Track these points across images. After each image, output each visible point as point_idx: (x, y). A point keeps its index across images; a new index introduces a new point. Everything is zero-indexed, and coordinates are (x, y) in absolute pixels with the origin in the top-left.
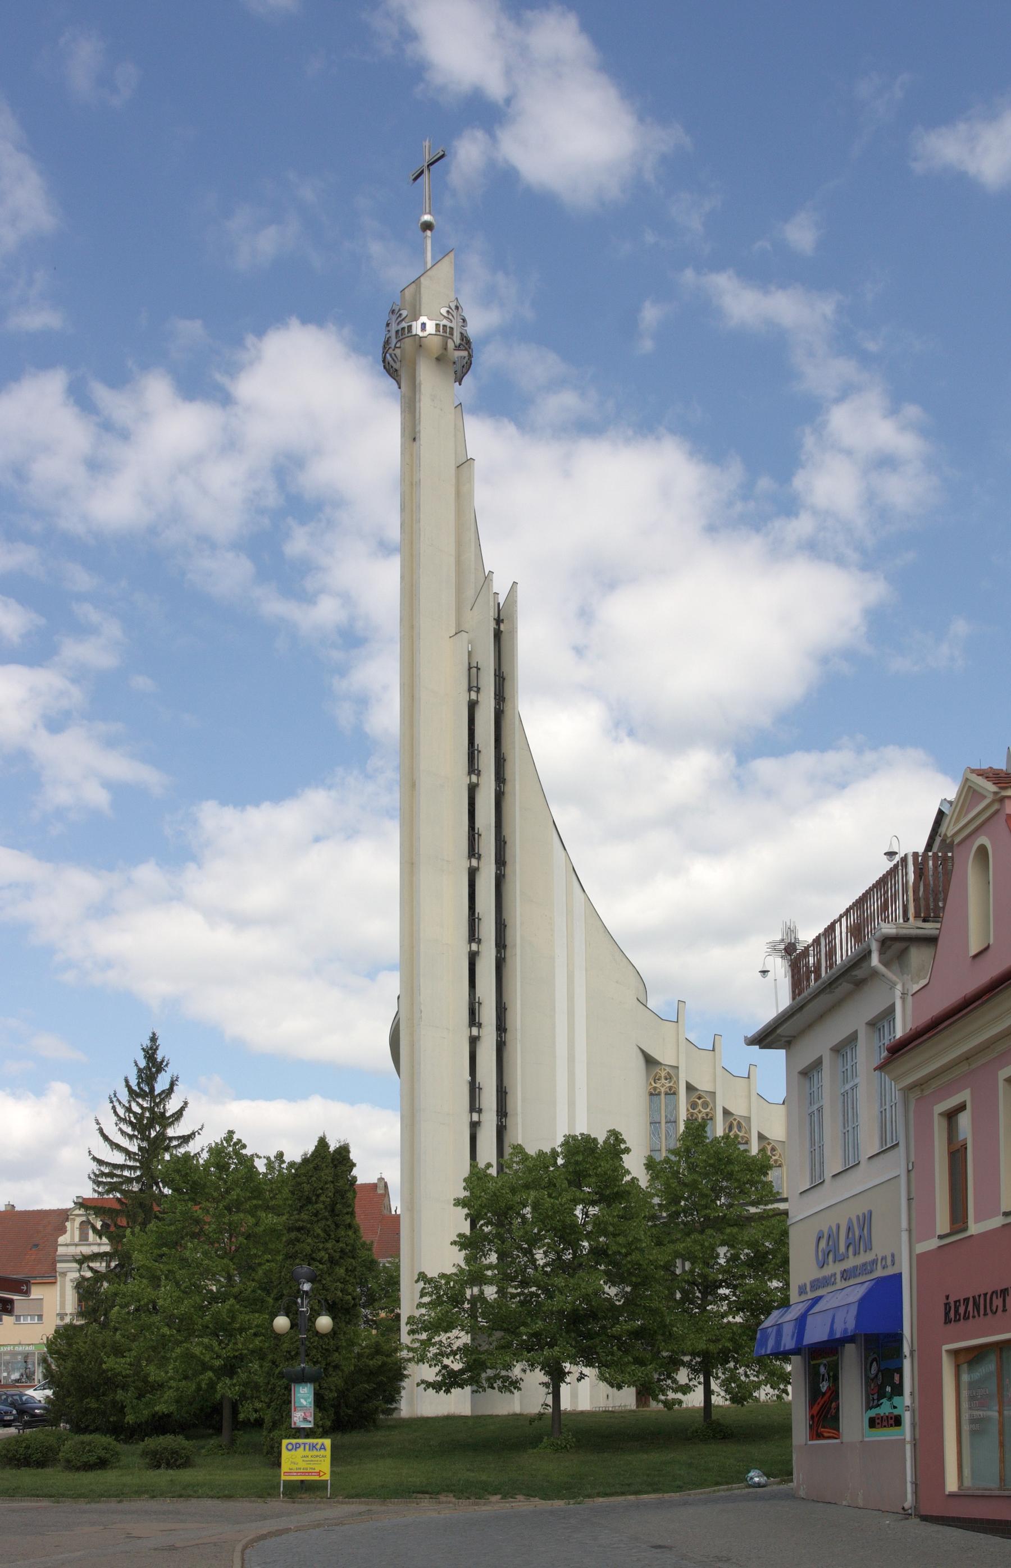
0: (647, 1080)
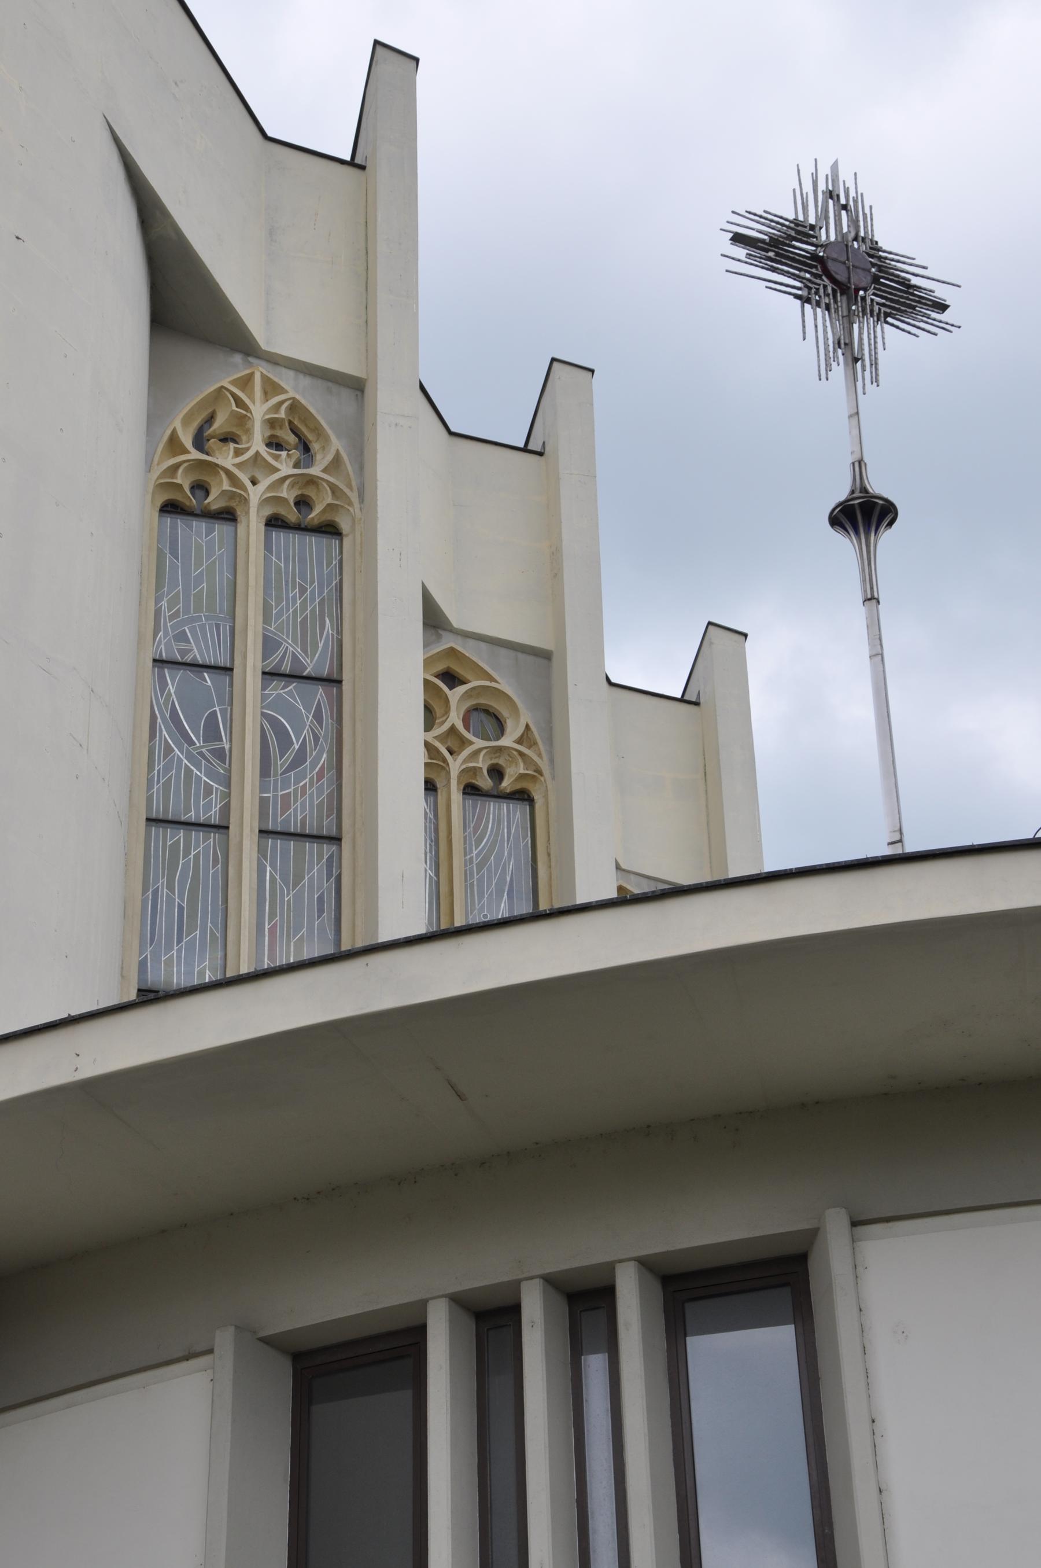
0: (154, 417)
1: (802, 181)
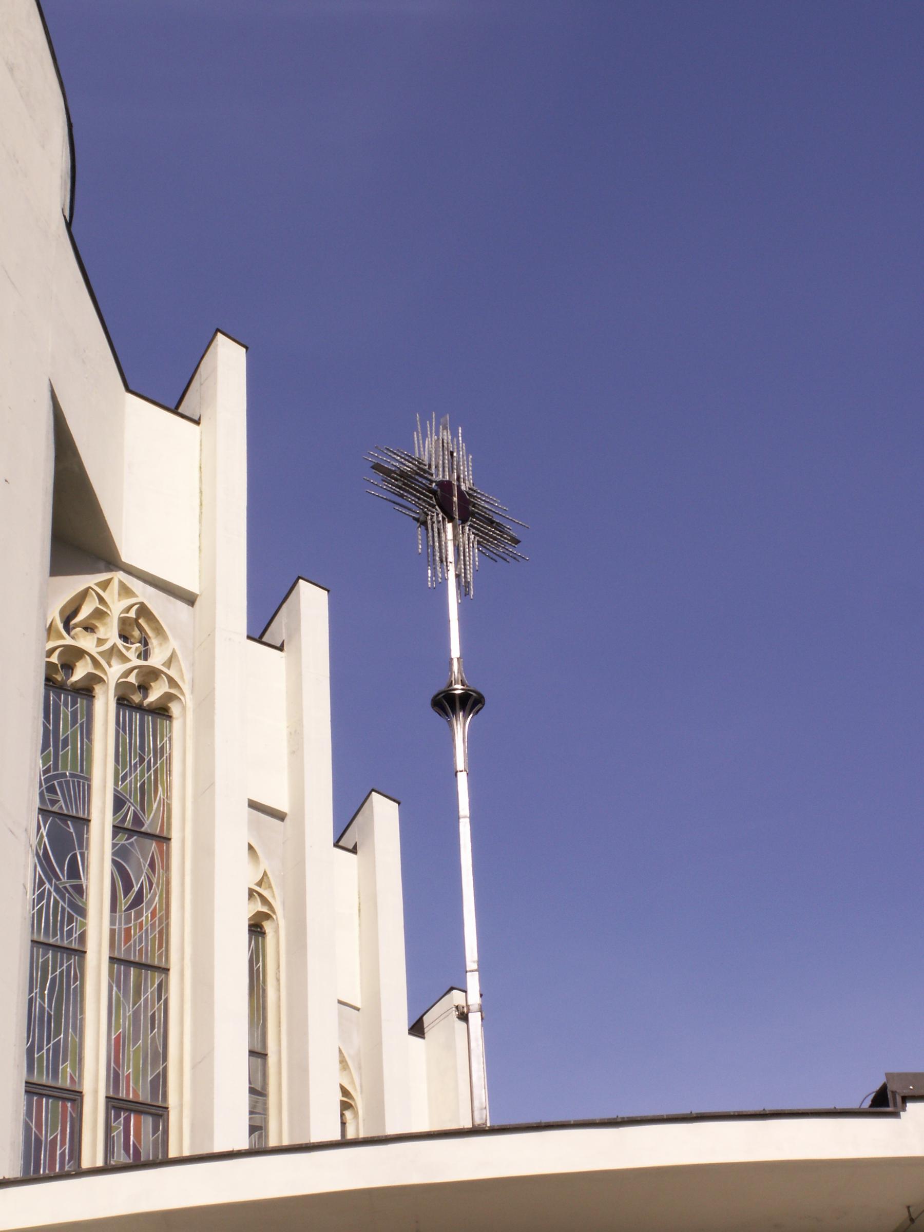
1: (70, 113)
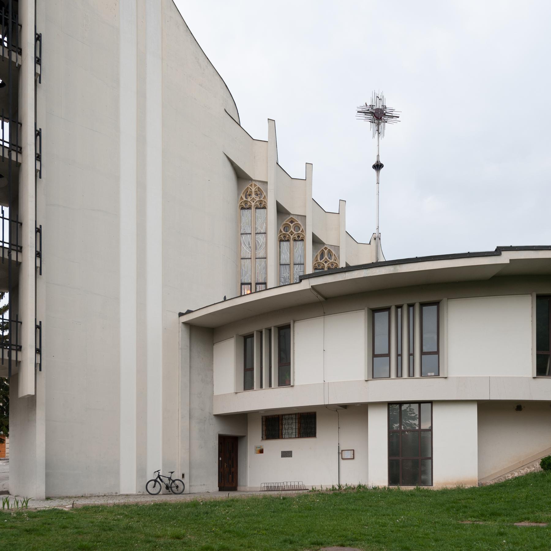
0: (238, 194)
